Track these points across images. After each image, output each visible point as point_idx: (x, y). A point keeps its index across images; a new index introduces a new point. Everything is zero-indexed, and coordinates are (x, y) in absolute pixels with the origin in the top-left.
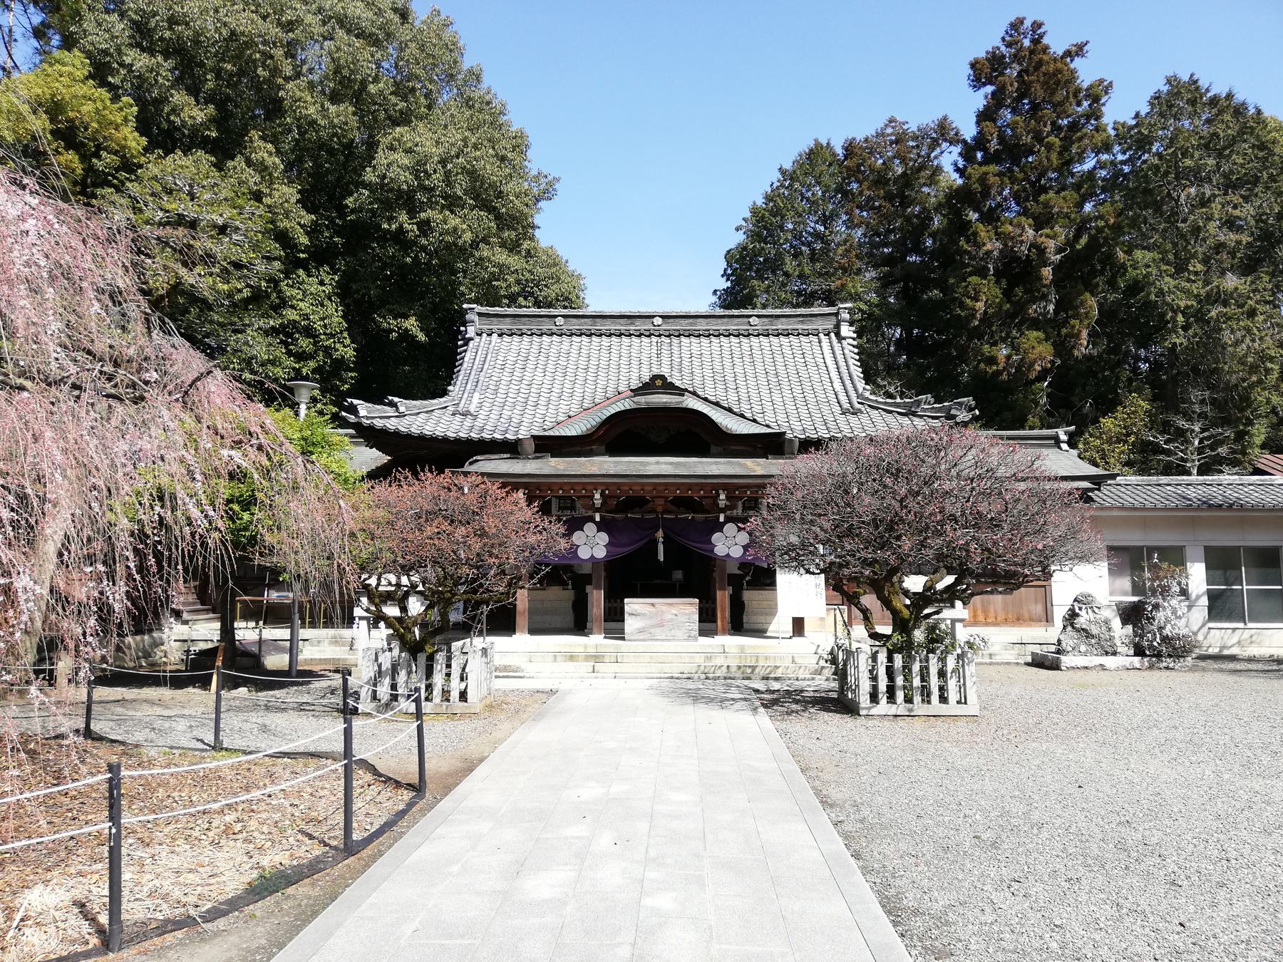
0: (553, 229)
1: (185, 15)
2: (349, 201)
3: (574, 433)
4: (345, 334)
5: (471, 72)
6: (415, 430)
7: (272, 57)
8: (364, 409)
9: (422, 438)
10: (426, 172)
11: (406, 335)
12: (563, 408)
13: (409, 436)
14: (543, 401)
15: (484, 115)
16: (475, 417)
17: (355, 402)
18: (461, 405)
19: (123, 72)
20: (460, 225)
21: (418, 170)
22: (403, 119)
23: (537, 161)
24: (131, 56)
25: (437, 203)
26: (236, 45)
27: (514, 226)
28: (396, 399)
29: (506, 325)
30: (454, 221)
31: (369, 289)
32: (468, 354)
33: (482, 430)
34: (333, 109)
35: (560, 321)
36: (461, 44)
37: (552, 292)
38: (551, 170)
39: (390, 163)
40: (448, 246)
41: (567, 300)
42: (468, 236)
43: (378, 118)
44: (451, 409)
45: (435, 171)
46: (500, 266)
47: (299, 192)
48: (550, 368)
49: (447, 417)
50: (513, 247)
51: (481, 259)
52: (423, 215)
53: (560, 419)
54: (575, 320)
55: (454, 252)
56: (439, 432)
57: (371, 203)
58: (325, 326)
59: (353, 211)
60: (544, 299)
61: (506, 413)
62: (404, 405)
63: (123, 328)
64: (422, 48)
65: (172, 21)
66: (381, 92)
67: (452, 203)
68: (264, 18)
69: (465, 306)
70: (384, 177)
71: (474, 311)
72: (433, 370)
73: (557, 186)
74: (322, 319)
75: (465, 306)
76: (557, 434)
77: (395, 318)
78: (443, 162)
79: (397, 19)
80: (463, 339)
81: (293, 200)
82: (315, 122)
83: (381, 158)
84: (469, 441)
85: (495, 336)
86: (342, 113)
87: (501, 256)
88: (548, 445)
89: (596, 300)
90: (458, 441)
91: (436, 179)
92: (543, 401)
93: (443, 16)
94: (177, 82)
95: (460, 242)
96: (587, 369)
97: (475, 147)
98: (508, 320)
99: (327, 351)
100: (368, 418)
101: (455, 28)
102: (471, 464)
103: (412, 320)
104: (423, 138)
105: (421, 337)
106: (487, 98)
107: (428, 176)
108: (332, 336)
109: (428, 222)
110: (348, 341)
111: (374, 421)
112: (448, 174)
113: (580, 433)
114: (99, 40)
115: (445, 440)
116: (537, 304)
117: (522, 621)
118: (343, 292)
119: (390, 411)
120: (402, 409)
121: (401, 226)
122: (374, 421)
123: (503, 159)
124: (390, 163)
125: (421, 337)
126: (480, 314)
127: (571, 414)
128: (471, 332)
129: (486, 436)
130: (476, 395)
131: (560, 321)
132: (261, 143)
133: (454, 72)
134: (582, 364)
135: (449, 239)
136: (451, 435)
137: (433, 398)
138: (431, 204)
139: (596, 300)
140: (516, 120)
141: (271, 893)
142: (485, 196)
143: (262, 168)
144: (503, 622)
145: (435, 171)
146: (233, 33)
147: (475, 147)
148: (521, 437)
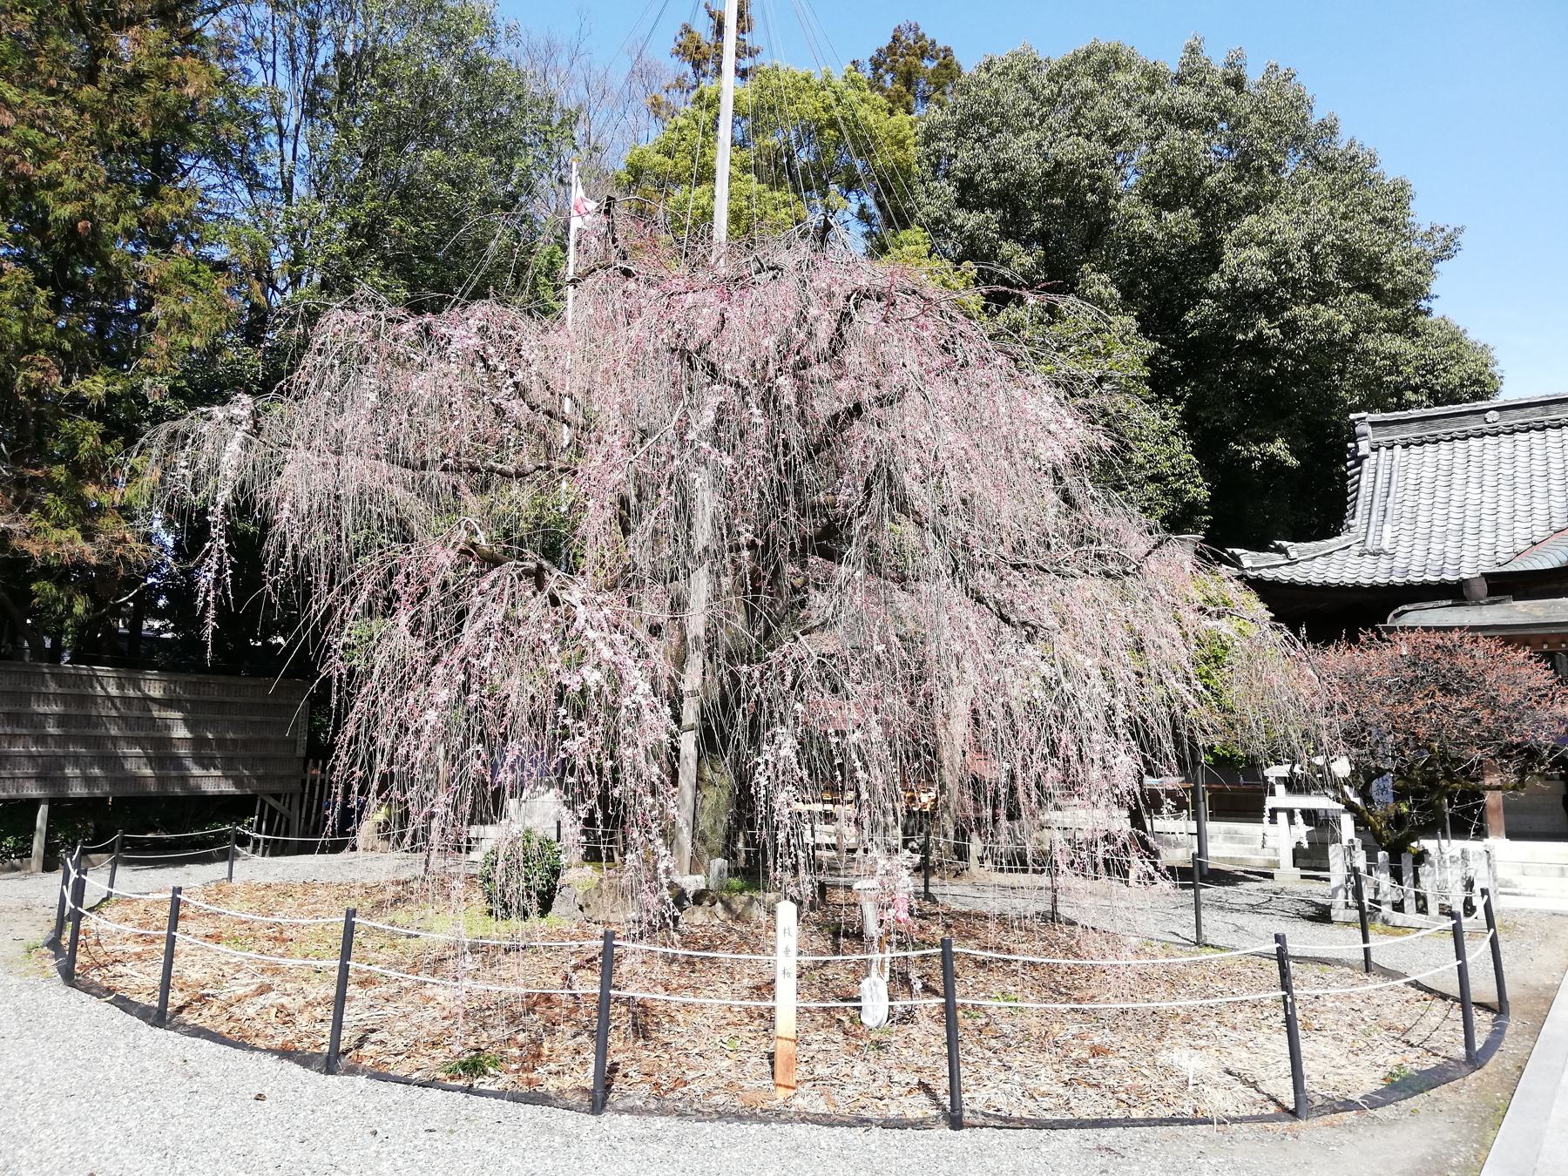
0: (1453, 299)
1: (1010, 160)
2: (1190, 317)
3: (1548, 566)
4: (1197, 472)
5: (1322, 125)
6: (1315, 579)
7: (1100, 178)
8: (1248, 558)
9: (1325, 588)
10: (1287, 262)
11: (1272, 462)
12: (1521, 532)
13: (1308, 587)
14: (1487, 525)
15: (1348, 175)
16: (1393, 556)
17: (1237, 551)
18: (1369, 542)
19: (954, 235)
20: (1335, 316)
21: (1279, 260)
22: (1253, 204)
23: (1423, 214)
24: (960, 217)
25: (1304, 296)
26: (1059, 176)
27: (1400, 301)
28: (1285, 544)
29: (1412, 432)
30: (1326, 314)
31: (1221, 414)
32: (1364, 476)
33: (1442, 571)
34: (1169, 216)
35: (1492, 416)
36: (1308, 95)
37: (1455, 376)
38: (1449, 221)
39: (1244, 261)
40: (1320, 347)
41: (1480, 387)
42: (1347, 329)
43: (1217, 211)
44: (1356, 549)
45: (1299, 259)
46: (1394, 357)
47: (1137, 319)
48: (1489, 480)
49: (1353, 559)
50: (1403, 327)
51: (1365, 352)
52: (1287, 315)
53: (1520, 548)
54: (1516, 412)
55: (1333, 350)
56: (1348, 578)
57: (1219, 313)
58: (1173, 467)
59: (1193, 327)
60: (1453, 393)
61: (1436, 547)
62: (1295, 549)
63: (337, 498)
64: (1266, 116)
65: (998, 168)
66: (1222, 183)
67: (1323, 293)
68: (1088, 137)
69: (1352, 416)
70: (1235, 279)
71: (1364, 420)
72: (1321, 505)
73: (1461, 238)
74: (1169, 459)
75: (1352, 416)
76: (1521, 568)
77: (1257, 443)
78: (1308, 245)
79: (1231, 92)
80: (1354, 457)
81: (1134, 330)
82: (1150, 237)
83: (1230, 258)
84: (1391, 588)
85: (1398, 448)
86: (1181, 220)
87: (1395, 344)
88: (1505, 585)
89: (1518, 383)
90: (1375, 588)
91: (1302, 268)
92: (1487, 525)
93: (1282, 71)
94: (1006, 235)
95: (1337, 337)
96: (1547, 475)
97: (1345, 217)
98: (1414, 425)
99: (1177, 494)
100: (1253, 569)
101: (1298, 78)
102: (1396, 616)
103: (1279, 442)
104: (1280, 223)
105: (1293, 462)
106: (1351, 152)
107: (1291, 266)
108: (1181, 476)
109: (1294, 320)
110: (1200, 480)
111: (1262, 572)
112: (1314, 257)
113: (1557, 564)
114: (934, 209)
115: (1357, 588)
116: (1436, 398)
117: (1495, 821)
118: (1190, 423)
119: (1279, 559)
120: (1293, 554)
121: (1260, 333)
122: (1262, 572)
123: (1382, 221)
124: (1244, 261)
125: (1293, 462)
126: (1373, 424)
127: (1536, 539)
128: (1364, 447)
129: (1415, 578)
130: (1387, 528)
131: (1492, 416)
132: (1094, 276)
133: (1303, 132)
134: (1538, 468)
135: (1323, 336)
136: (1365, 581)
137: (1308, 541)
138: (1297, 298)
139: (1518, 383)
140: (1390, 170)
141: (1416, 1093)
142: (1363, 273)
143: (1098, 301)
144: (1467, 824)
145: (1299, 259)
146: (1058, 164)
147: (1345, 217)
148: (1466, 577)
